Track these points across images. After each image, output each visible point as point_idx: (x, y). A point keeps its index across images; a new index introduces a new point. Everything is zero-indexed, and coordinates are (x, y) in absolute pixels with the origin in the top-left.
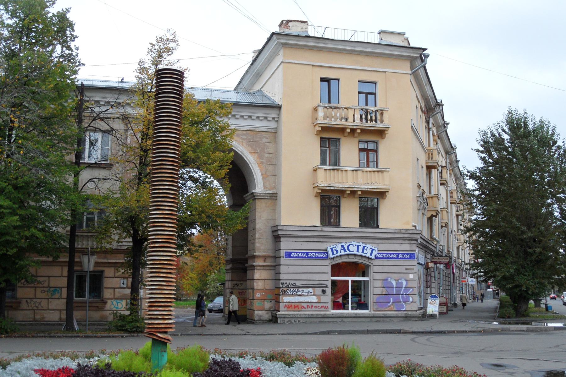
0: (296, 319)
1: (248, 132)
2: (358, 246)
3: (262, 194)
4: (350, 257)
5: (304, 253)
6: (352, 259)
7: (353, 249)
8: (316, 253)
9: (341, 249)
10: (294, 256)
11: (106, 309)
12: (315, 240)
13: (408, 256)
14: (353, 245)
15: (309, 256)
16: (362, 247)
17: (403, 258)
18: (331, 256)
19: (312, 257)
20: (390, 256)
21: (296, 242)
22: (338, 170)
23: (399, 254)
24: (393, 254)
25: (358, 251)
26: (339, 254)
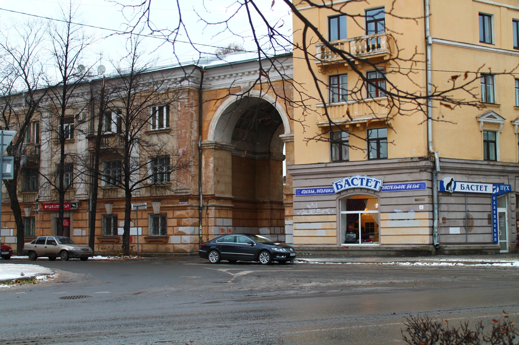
0: (306, 252)
1: (277, 82)
2: (362, 179)
3: (288, 138)
4: (356, 190)
5: (313, 189)
6: (358, 192)
7: (357, 182)
8: (323, 189)
9: (345, 184)
10: (304, 193)
11: (168, 243)
12: (323, 176)
13: (418, 186)
14: (357, 178)
15: (317, 192)
16: (366, 180)
17: (412, 189)
18: (336, 191)
19: (320, 193)
20: (397, 187)
21: (307, 180)
22: (335, 106)
23: (407, 185)
24: (401, 185)
25: (362, 184)
26: (343, 188)
